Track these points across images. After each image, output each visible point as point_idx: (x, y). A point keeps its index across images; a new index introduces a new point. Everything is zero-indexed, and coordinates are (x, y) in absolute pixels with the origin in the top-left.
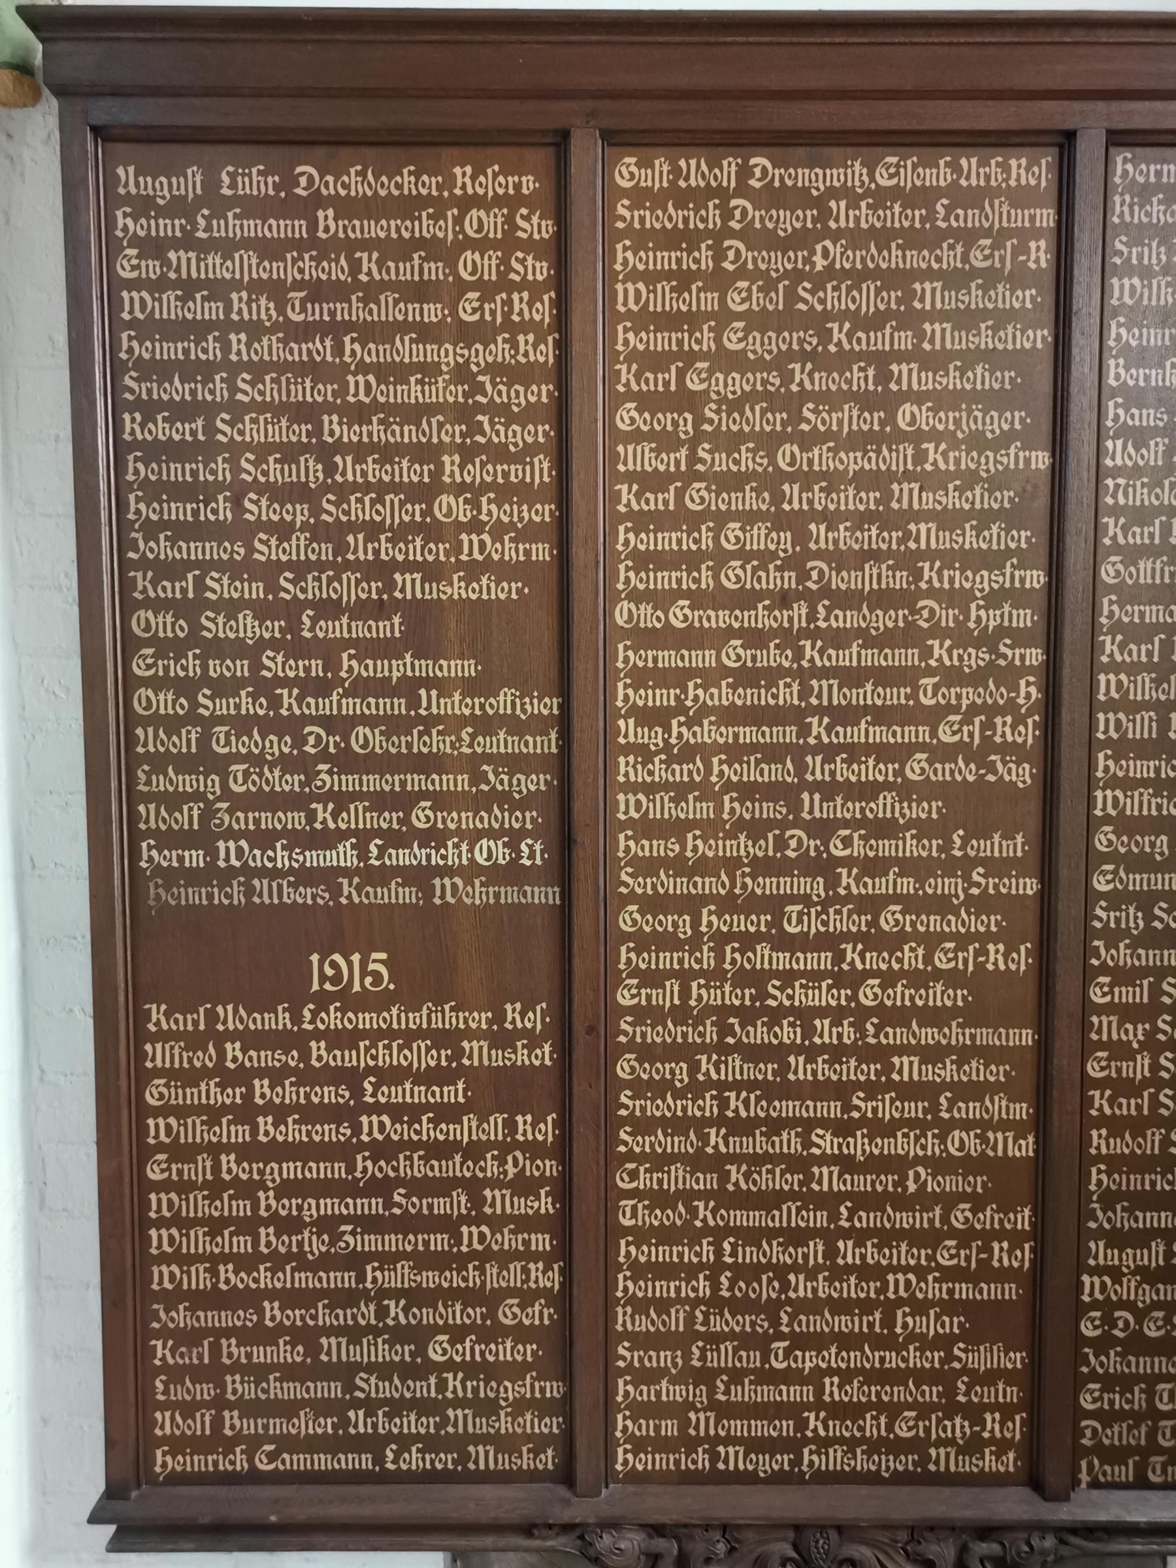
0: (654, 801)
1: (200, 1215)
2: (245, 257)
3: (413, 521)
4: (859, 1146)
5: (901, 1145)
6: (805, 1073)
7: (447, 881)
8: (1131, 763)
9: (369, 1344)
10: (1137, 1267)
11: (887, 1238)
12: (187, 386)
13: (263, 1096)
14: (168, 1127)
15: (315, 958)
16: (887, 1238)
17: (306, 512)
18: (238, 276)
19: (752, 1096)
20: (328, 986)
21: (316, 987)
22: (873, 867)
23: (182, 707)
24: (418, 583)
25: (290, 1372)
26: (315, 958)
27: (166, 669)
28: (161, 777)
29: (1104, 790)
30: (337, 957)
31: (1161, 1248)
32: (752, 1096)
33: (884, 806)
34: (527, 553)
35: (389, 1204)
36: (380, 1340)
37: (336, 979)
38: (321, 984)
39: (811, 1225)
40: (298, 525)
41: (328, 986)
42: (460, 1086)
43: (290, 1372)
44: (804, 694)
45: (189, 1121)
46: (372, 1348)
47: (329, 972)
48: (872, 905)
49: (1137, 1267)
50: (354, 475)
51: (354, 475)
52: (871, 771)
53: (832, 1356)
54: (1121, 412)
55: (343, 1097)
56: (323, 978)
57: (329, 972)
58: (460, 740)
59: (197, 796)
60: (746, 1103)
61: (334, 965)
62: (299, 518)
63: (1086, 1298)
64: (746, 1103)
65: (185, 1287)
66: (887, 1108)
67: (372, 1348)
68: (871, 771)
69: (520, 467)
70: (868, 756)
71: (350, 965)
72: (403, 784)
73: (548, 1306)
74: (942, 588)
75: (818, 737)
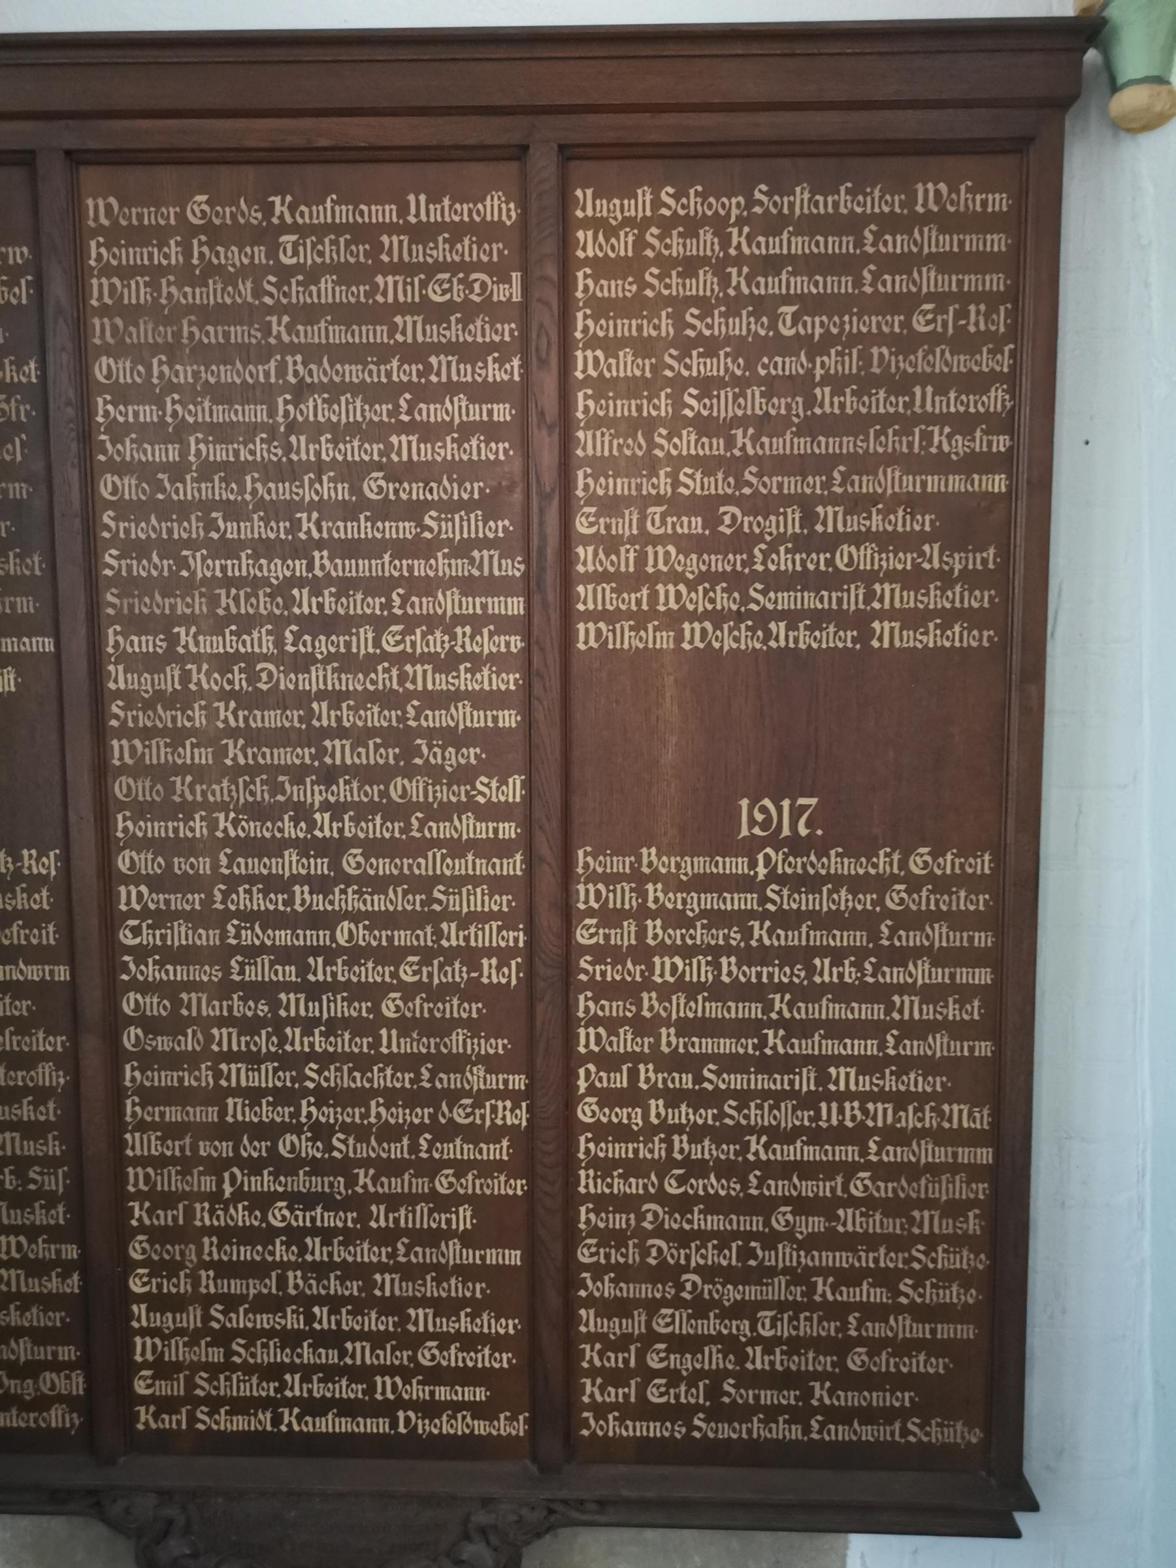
0: (614, 891)
6: (308, 453)
10: (624, 218)
13: (655, 936)
15: (744, 803)
19: (242, 593)
20: (757, 831)
21: (745, 832)
23: (165, 1008)
24: (302, 1002)
26: (744, 803)
29: (586, 1027)
30: (767, 802)
31: (648, 197)
32: (242, 593)
37: (765, 825)
38: (750, 828)
39: (235, 1258)
41: (757, 831)
44: (869, 596)
47: (759, 817)
49: (624, 218)
55: (798, 976)
56: (752, 822)
57: (759, 817)
60: (236, 599)
61: (764, 810)
63: (138, 1358)
64: (236, 599)
70: (341, 1377)
71: (780, 810)
72: (390, 939)
73: (23, 402)
74: (239, 614)
75: (780, 1013)
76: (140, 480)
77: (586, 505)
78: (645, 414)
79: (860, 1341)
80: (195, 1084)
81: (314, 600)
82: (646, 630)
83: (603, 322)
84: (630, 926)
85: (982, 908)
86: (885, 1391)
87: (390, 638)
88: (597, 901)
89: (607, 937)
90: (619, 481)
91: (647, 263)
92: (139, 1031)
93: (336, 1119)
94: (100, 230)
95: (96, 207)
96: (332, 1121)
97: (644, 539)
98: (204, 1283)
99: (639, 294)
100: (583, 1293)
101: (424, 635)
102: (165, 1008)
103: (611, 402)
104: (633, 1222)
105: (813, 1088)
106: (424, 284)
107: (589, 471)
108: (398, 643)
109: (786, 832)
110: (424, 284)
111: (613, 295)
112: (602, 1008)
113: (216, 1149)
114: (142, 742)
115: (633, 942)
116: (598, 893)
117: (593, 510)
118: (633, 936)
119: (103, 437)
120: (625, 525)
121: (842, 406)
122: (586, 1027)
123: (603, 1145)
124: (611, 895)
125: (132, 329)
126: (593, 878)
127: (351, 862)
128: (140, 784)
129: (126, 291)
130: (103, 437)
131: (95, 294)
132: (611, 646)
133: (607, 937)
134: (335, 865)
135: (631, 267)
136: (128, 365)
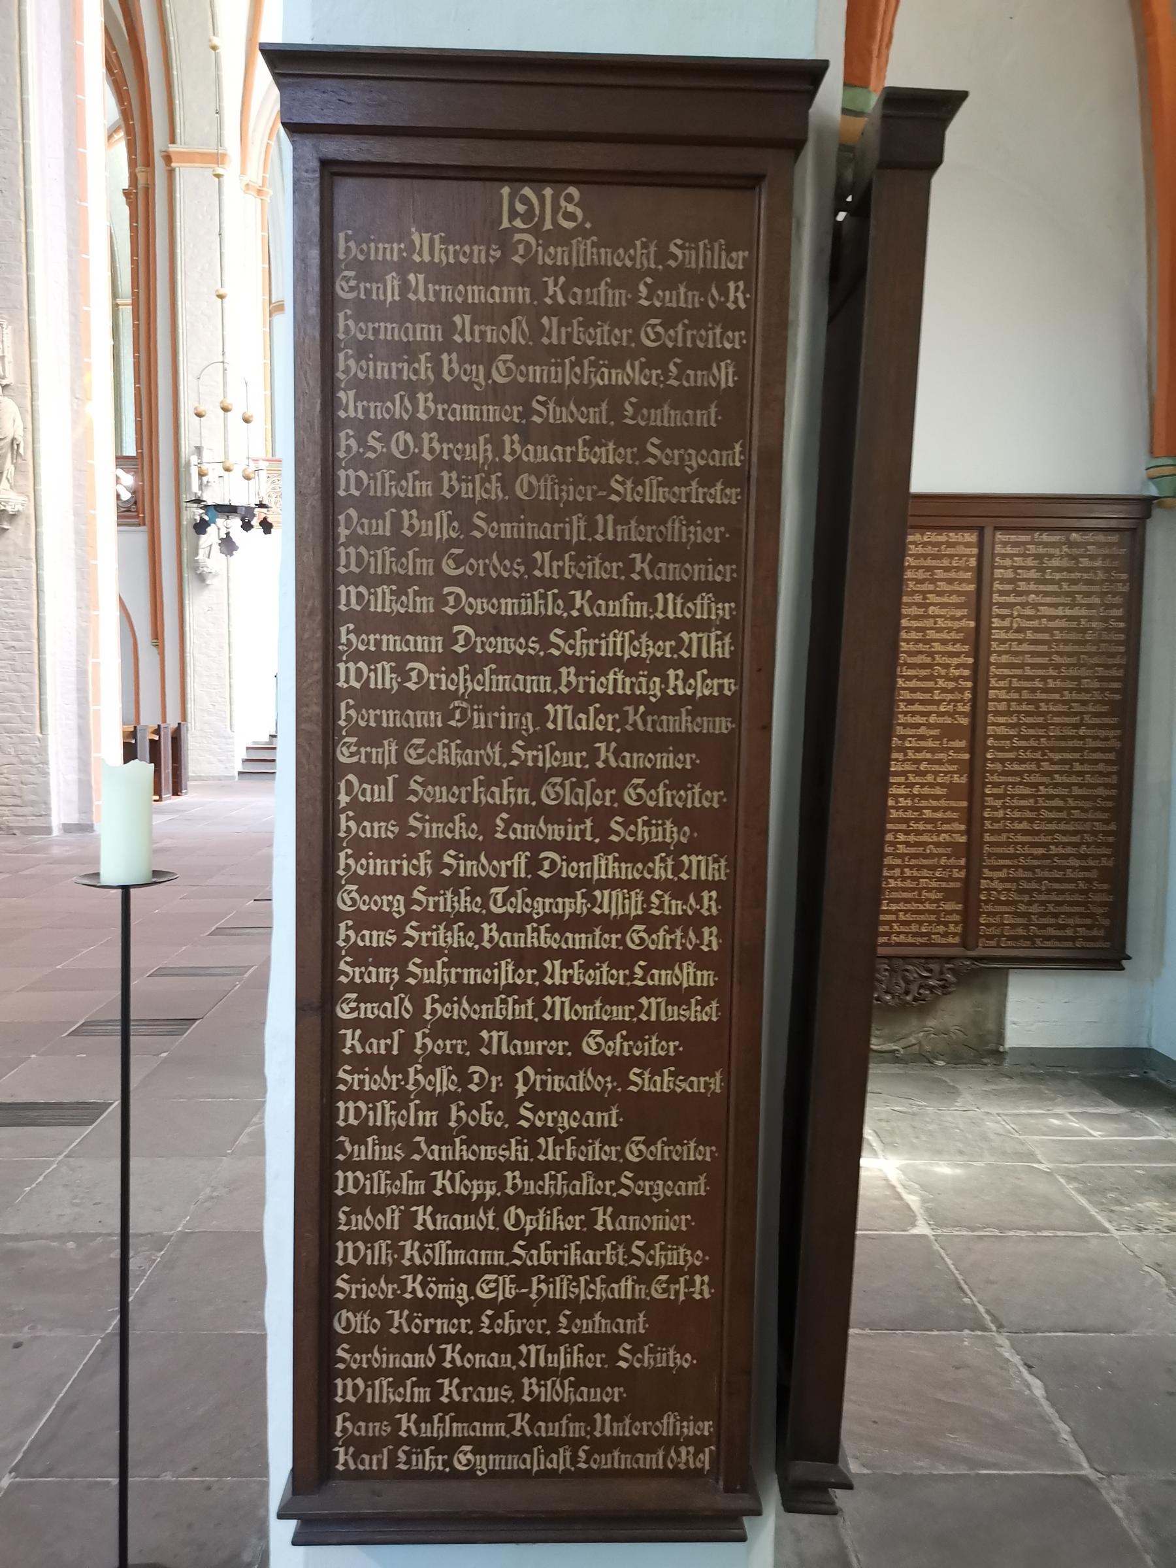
1: (384, 1401)
4: (912, 838)
5: (925, 838)
8: (372, 245)
11: (919, 867)
14: (356, 1251)
16: (919, 867)
21: (505, 224)
22: (918, 750)
29: (346, 662)
33: (922, 731)
41: (518, 223)
47: (520, 208)
48: (917, 762)
52: (919, 720)
53: (902, 906)
54: (352, 712)
56: (513, 214)
57: (520, 208)
61: (525, 200)
66: (921, 826)
68: (919, 720)
77: (346, 269)
78: (405, 378)
79: (652, 312)
82: (407, 595)
83: (363, 861)
84: (392, 281)
85: (717, 540)
86: (665, 1214)
89: (368, 756)
90: (379, 364)
91: (409, 954)
94: (348, 1268)
95: (345, 1386)
97: (405, 771)
99: (400, 837)
100: (341, 1157)
102: (375, 1326)
103: (371, 363)
104: (396, 977)
105: (583, 538)
107: (352, 702)
109: (548, 225)
111: (375, 944)
112: (363, 938)
115: (397, 298)
116: (359, 672)
117: (354, 740)
118: (396, 293)
120: (385, 754)
121: (570, 978)
122: (346, 662)
123: (363, 861)
124: (372, 674)
126: (356, 656)
132: (372, 609)
133: (368, 756)
134: (576, 1047)
135: (395, 956)
136: (366, 1318)
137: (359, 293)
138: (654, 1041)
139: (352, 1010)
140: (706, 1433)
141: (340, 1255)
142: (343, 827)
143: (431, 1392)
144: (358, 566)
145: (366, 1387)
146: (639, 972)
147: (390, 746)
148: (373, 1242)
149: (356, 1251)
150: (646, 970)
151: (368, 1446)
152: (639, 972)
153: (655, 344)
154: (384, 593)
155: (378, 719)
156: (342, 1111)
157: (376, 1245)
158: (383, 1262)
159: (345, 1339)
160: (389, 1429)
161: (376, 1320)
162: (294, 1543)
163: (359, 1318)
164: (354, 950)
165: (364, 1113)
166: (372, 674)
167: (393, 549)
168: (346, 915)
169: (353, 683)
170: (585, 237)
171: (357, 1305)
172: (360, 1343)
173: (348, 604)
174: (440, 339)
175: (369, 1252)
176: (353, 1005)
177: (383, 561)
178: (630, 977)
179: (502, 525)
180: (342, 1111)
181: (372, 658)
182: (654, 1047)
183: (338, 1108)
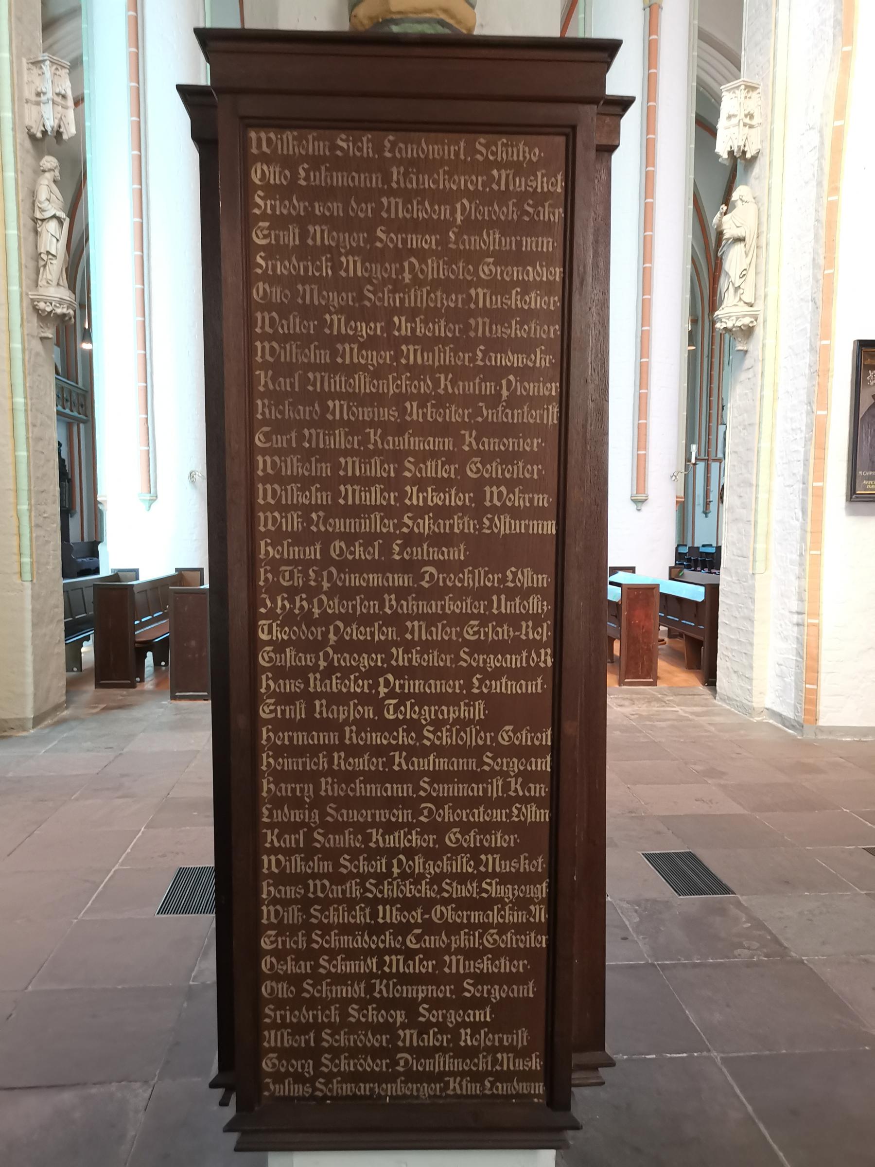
2: (362, 377)
3: (493, 1045)
7: (494, 489)
9: (440, 352)
12: (311, 1013)
17: (403, 1016)
18: (357, 391)
23: (292, 992)
25: (370, 777)
27: (284, 943)
28: (279, 812)
34: (531, 500)
35: (481, 763)
36: (447, 349)
40: (398, 1024)
42: (539, 681)
43: (370, 777)
45: (289, 487)
46: (442, 354)
50: (418, 416)
51: (418, 416)
54: (270, 576)
58: (505, 576)
59: (303, 824)
62: (399, 1020)
65: (284, 529)
67: (442, 354)
69: (516, 441)
76: (283, 168)
80: (314, 768)
81: (409, 325)
87: (469, 629)
88: (276, 918)
92: (274, 960)
93: (442, 304)
94: (271, 875)
95: (270, 861)
96: (439, 305)
98: (323, 787)
101: (494, 628)
102: (292, 992)
106: (481, 936)
108: (475, 633)
110: (481, 936)
113: (329, 209)
114: (280, 513)
119: (264, 596)
123: (280, 760)
125: (284, 322)
127: (451, 838)
128: (272, 170)
129: (283, 464)
130: (264, 596)
131: (266, 866)
134: (440, 840)
136: (277, 169)
137: (276, 714)
138: (499, 835)
139: (271, 711)
140: (540, 870)
141: (266, 866)
142: (265, 736)
143: (330, 354)
144: (273, 498)
145: (282, 490)
146: (488, 1084)
147: (294, 231)
148: (287, 513)
149: (278, 862)
150: (485, 353)
151: (287, 699)
152: (488, 1084)
153: (489, 278)
154: (292, 490)
155: (291, 739)
156: (262, 519)
157: (293, 858)
158: (298, 871)
159: (270, 1001)
160: (302, 686)
161: (292, 988)
162: (237, 1150)
163: (280, 986)
164: (274, 747)
165: (283, 864)
166: (285, 914)
167: (302, 855)
168: (265, 670)
169: (270, 527)
170: (445, 1053)
171: (273, 280)
172: (280, 1004)
173: (264, 470)
174: (337, 742)
175: (283, 492)
176: (273, 939)
177: (293, 466)
178: (473, 359)
179: (381, 382)
180: (262, 519)
181: (284, 509)
182: (499, 840)
183: (256, 347)
